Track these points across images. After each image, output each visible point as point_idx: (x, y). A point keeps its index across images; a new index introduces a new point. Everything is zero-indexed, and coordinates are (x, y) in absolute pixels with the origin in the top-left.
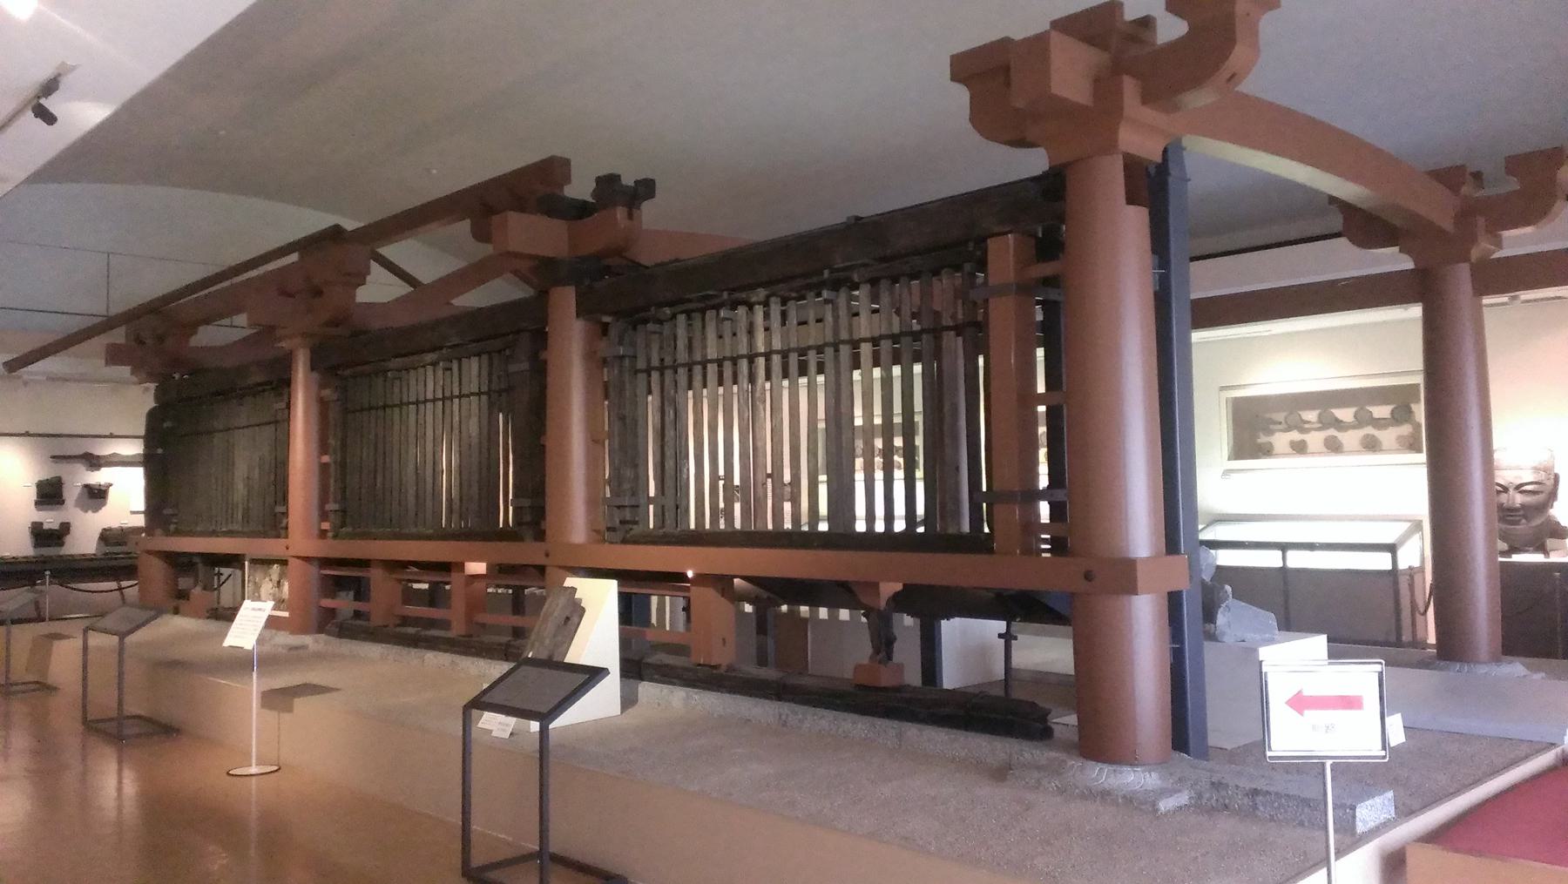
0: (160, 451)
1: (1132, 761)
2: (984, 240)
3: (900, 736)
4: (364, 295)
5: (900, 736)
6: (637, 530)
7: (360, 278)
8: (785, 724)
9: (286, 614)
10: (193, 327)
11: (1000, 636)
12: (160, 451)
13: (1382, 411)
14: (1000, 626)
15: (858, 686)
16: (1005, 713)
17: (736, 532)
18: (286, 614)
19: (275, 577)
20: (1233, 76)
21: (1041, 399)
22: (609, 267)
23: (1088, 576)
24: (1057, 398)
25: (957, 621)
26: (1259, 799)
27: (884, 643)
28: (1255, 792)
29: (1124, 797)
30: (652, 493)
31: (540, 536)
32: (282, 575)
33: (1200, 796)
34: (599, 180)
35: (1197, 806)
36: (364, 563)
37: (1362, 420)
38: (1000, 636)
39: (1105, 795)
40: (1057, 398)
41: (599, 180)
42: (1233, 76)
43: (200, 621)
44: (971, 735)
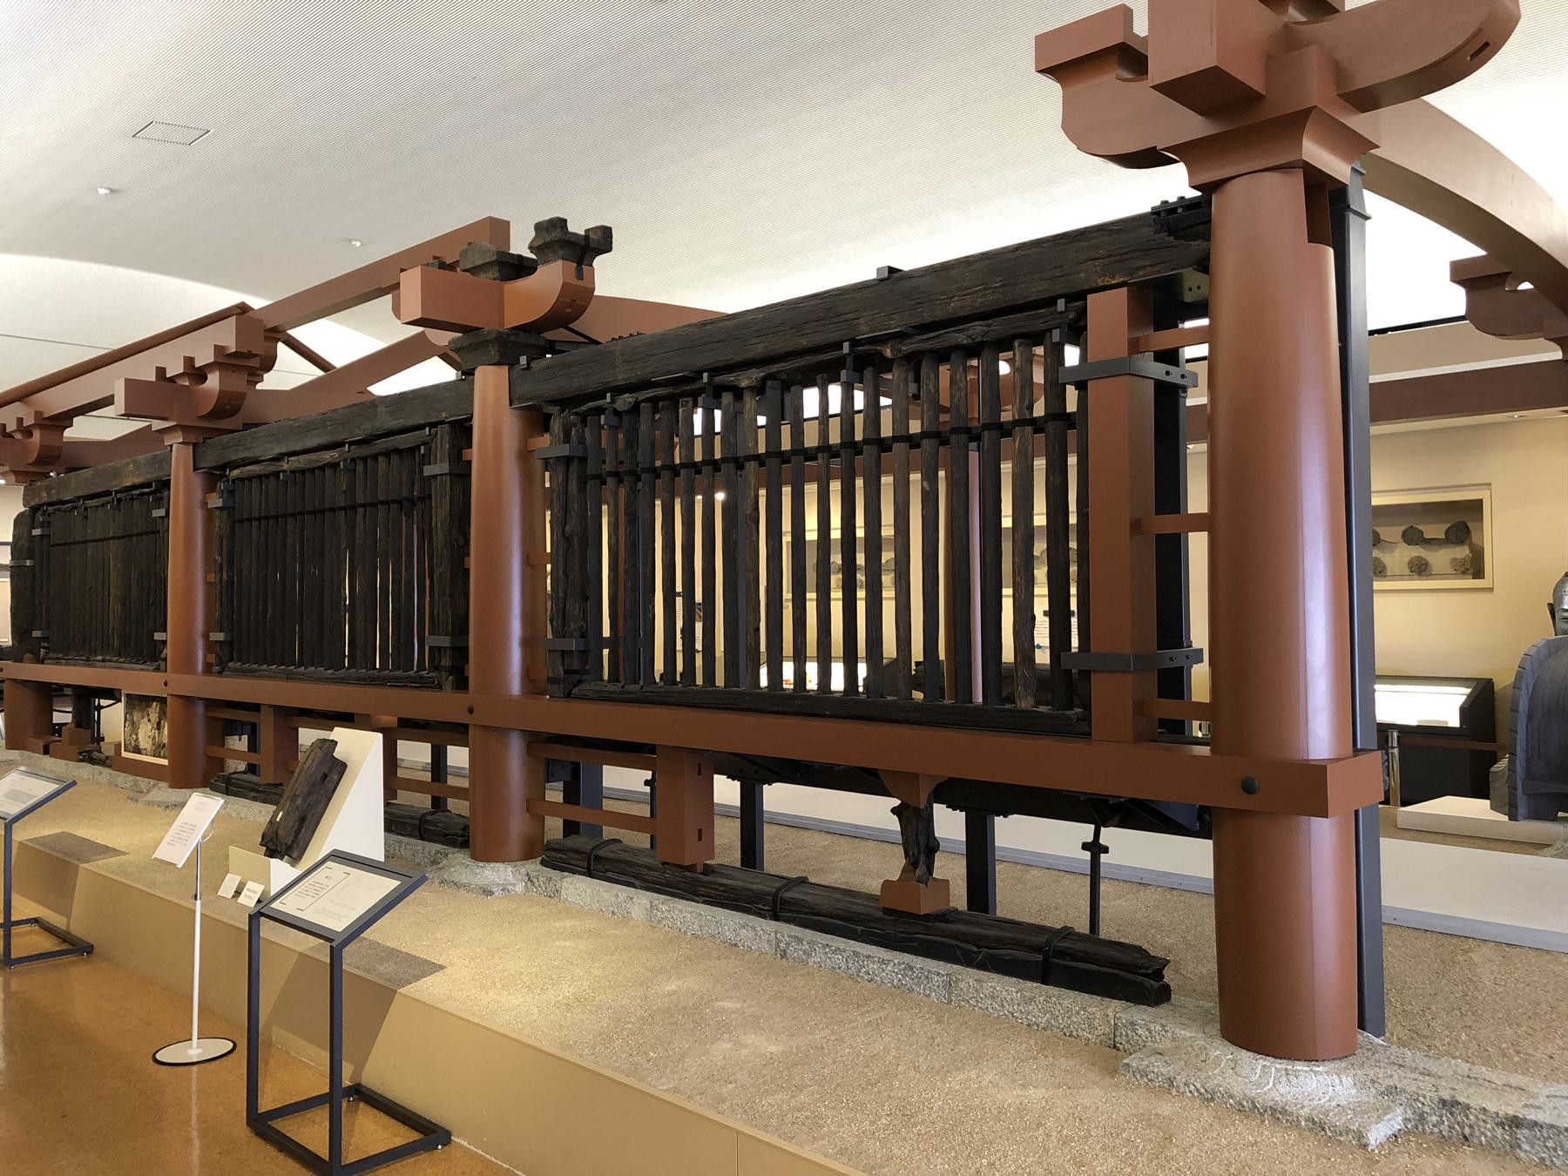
0: (28, 563)
1: (1310, 1056)
2: (1082, 296)
3: (949, 985)
4: (271, 381)
5: (949, 985)
6: (589, 687)
7: (269, 363)
8: (784, 955)
9: (165, 762)
10: (66, 418)
11: (1085, 846)
12: (28, 563)
13: (1434, 530)
14: (1086, 831)
15: (886, 911)
16: (1098, 966)
17: (718, 692)
18: (165, 762)
19: (154, 717)
20: (1487, 44)
21: (1199, 522)
22: (552, 342)
23: (1248, 788)
24: (1166, 524)
25: (1016, 819)
26: (1523, 1133)
27: (919, 843)
28: (1515, 1122)
29: (1310, 1119)
30: (606, 633)
31: (462, 684)
32: (163, 714)
33: (1422, 1118)
34: (539, 227)
35: (1414, 1132)
36: (256, 708)
37: (1412, 537)
38: (1085, 846)
39: (1277, 1114)
40: (1166, 524)
41: (539, 227)
42: (1487, 44)
43: (72, 764)
44: (1053, 990)
